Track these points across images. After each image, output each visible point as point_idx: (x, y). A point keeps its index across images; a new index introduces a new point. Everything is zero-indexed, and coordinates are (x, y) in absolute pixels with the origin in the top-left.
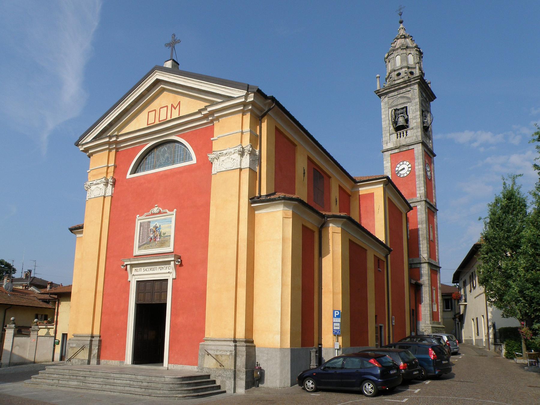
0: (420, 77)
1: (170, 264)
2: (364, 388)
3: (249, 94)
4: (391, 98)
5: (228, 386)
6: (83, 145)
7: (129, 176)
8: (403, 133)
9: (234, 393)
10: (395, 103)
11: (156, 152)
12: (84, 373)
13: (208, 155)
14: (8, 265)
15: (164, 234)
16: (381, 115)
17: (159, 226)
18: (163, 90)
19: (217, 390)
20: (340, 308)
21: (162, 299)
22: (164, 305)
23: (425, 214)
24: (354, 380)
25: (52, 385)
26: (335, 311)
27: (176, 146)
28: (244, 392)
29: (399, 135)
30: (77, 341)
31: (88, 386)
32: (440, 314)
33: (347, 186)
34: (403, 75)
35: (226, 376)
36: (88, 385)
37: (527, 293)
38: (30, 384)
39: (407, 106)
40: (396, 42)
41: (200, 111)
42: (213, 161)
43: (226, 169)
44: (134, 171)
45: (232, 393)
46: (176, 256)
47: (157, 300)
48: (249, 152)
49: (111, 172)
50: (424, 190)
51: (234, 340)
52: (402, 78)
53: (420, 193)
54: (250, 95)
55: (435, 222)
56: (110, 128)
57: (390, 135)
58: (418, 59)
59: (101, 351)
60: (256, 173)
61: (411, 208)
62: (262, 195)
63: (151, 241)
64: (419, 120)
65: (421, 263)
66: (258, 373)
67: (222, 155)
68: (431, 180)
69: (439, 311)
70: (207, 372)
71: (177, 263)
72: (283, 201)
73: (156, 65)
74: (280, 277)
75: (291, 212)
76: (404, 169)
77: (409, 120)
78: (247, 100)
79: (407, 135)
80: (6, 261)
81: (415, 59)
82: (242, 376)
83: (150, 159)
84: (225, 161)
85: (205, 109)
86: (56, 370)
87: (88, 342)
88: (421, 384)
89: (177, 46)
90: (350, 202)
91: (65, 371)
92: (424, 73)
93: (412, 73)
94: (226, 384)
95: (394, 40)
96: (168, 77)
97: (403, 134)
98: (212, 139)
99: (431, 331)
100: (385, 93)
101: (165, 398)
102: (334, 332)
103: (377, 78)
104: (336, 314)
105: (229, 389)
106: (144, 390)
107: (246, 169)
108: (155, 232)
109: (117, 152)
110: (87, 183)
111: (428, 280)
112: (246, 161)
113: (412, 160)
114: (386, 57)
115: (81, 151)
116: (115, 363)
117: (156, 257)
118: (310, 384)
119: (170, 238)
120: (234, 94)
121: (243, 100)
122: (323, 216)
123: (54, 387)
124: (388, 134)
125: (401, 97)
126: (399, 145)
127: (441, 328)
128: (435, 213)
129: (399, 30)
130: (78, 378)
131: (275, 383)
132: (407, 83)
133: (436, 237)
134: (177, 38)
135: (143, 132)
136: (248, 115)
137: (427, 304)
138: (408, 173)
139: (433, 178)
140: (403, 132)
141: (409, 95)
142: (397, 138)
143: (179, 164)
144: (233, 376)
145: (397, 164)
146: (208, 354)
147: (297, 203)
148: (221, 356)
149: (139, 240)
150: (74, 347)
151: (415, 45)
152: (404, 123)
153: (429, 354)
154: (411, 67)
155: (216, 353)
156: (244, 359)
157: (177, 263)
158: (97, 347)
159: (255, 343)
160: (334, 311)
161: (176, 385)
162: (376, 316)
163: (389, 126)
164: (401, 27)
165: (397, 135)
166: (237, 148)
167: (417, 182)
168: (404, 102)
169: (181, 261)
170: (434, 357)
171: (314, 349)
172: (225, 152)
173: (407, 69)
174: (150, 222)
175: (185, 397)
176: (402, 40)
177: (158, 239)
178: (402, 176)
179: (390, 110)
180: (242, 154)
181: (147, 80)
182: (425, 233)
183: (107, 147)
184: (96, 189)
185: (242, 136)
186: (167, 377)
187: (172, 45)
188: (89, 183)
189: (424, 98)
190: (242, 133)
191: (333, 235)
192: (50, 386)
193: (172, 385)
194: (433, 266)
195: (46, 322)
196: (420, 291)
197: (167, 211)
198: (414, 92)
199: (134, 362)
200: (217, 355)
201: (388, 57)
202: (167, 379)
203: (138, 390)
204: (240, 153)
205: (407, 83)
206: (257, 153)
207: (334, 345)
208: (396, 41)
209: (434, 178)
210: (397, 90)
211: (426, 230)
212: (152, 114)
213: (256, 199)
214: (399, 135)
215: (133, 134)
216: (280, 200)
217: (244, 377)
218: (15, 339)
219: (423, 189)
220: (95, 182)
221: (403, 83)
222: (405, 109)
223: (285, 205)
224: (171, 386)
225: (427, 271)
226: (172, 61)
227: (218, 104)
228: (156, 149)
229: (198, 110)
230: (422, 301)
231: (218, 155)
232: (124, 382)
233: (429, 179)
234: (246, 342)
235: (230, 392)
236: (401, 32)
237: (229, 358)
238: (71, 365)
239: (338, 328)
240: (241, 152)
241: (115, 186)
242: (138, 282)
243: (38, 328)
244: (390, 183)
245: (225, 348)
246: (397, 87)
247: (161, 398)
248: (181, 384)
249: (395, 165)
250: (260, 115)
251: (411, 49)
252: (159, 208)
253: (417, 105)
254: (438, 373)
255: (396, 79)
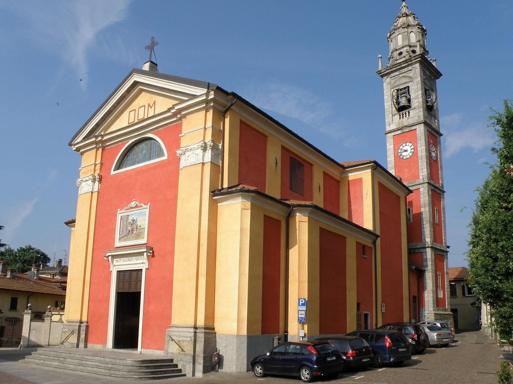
0: (420, 56)
1: (143, 255)
2: (301, 374)
3: (210, 92)
4: (393, 78)
5: (188, 370)
6: (75, 145)
7: (112, 173)
8: (406, 114)
9: (192, 376)
10: (398, 83)
11: (137, 149)
12: (65, 355)
13: (176, 151)
14: (43, 255)
15: (140, 226)
16: (384, 96)
17: (135, 219)
18: (142, 91)
19: (178, 372)
20: (306, 297)
21: (138, 288)
22: (139, 293)
23: (428, 197)
24: (294, 367)
25: (38, 365)
26: (300, 300)
27: (152, 143)
28: (202, 376)
29: (401, 116)
30: (68, 326)
31: (65, 367)
32: (446, 301)
33: (335, 173)
34: (404, 54)
35: (187, 360)
36: (66, 365)
37: (479, 280)
38: (23, 363)
39: (409, 85)
40: (398, 21)
41: (169, 110)
42: (181, 156)
43: (191, 164)
44: (118, 167)
45: (191, 376)
46: (148, 247)
47: (134, 289)
48: (211, 147)
49: (98, 169)
50: (426, 172)
51: (194, 327)
52: (404, 57)
53: (422, 175)
54: (211, 93)
55: (442, 204)
56: (97, 128)
57: (392, 116)
58: (421, 36)
59: (88, 335)
60: (219, 167)
61: (411, 192)
62: (224, 187)
63: (129, 233)
64: (421, 99)
65: (425, 248)
66: (216, 358)
67: (188, 151)
68: (436, 161)
69: (446, 298)
70: (171, 357)
71: (149, 254)
72: (240, 193)
73: (134, 68)
74: (238, 267)
75: (250, 204)
76: (406, 151)
77: (411, 100)
78: (208, 98)
79: (409, 115)
80: (41, 251)
81: (417, 37)
82: (200, 361)
83: (131, 156)
84: (190, 157)
85: (173, 108)
86: (45, 352)
87: (77, 327)
88: (375, 371)
89: (156, 48)
90: (339, 188)
91: (52, 353)
92: (428, 51)
93: (414, 52)
94: (186, 368)
95: (396, 18)
96: (144, 79)
97: (400, 117)
98: (180, 136)
99: (434, 319)
100: (387, 73)
101: (123, 378)
102: (299, 319)
103: (379, 58)
104: (301, 303)
105: (189, 373)
106: (107, 370)
107: (208, 163)
108: (132, 225)
109: (103, 150)
110: (78, 180)
111: (431, 266)
112: (209, 155)
113: (414, 141)
114: (388, 36)
115: (74, 150)
116: (98, 347)
117: (132, 249)
118: (259, 369)
119: (145, 231)
120: (197, 92)
121: (204, 98)
122: (288, 206)
123: (40, 366)
124: (391, 115)
125: (403, 77)
126: (401, 126)
127: (447, 314)
128: (442, 195)
129: (401, 8)
130: (60, 359)
131: (232, 368)
132: (408, 62)
133: (442, 220)
134: (155, 40)
135: (124, 130)
136: (211, 111)
137: (430, 290)
138: (411, 154)
139: (439, 159)
140: (405, 112)
141: (411, 74)
142: (400, 119)
143: (154, 160)
144: (192, 361)
145: (400, 145)
146: (173, 340)
147: (254, 194)
148: (183, 341)
149: (120, 232)
150: (66, 332)
151: (417, 22)
152: (406, 103)
153: (384, 342)
154: (413, 45)
155: (178, 339)
156: (202, 345)
157: (149, 254)
158: (85, 332)
159: (216, 330)
160: (299, 300)
161: (135, 368)
162: (358, 304)
163: (392, 107)
164: (403, 5)
165: (400, 116)
166: (200, 144)
167: (420, 164)
168: (406, 82)
169: (153, 252)
170: (389, 345)
171: (277, 336)
172: (189, 148)
173: (409, 47)
174: (128, 215)
175: (141, 378)
176: (404, 19)
177: (135, 231)
178: (405, 158)
179: (392, 90)
180: (205, 149)
181: (127, 82)
182: (428, 216)
183: (95, 146)
184: (86, 186)
185: (205, 132)
186: (128, 360)
187: (151, 48)
188: (79, 180)
189: (427, 76)
190: (205, 129)
191: (299, 223)
192: (37, 365)
193: (132, 367)
194: (437, 250)
195: (59, 309)
196: (424, 276)
197: (143, 205)
198: (415, 71)
199: (115, 346)
200: (179, 341)
201: (391, 36)
202: (128, 362)
203: (103, 371)
204: (202, 148)
205: (408, 62)
206: (220, 147)
207: (299, 333)
208: (398, 20)
209: (440, 159)
210: (398, 70)
211: (430, 214)
212: (132, 114)
213: (217, 192)
214: (401, 116)
215: (115, 133)
216: (238, 192)
217: (202, 361)
218: (31, 324)
219: (426, 170)
220: (84, 179)
221: (405, 62)
222: (407, 89)
223: (244, 197)
224: (131, 368)
225: (430, 255)
226: (150, 62)
227: (184, 103)
228: (135, 147)
229: (168, 109)
230: (425, 287)
231: (184, 151)
232: (94, 363)
233: (433, 160)
234: (205, 328)
235: (189, 375)
236: (404, 10)
237: (189, 344)
238: (63, 347)
239: (304, 316)
240: (203, 147)
241: (101, 183)
242: (119, 272)
243: (52, 314)
244: (378, 167)
245: (186, 334)
246: (399, 67)
247: (119, 379)
248: (140, 366)
249: (398, 147)
250: (224, 111)
251: (413, 27)
252: (136, 202)
253: (419, 84)
254: (393, 361)
255: (398, 58)
